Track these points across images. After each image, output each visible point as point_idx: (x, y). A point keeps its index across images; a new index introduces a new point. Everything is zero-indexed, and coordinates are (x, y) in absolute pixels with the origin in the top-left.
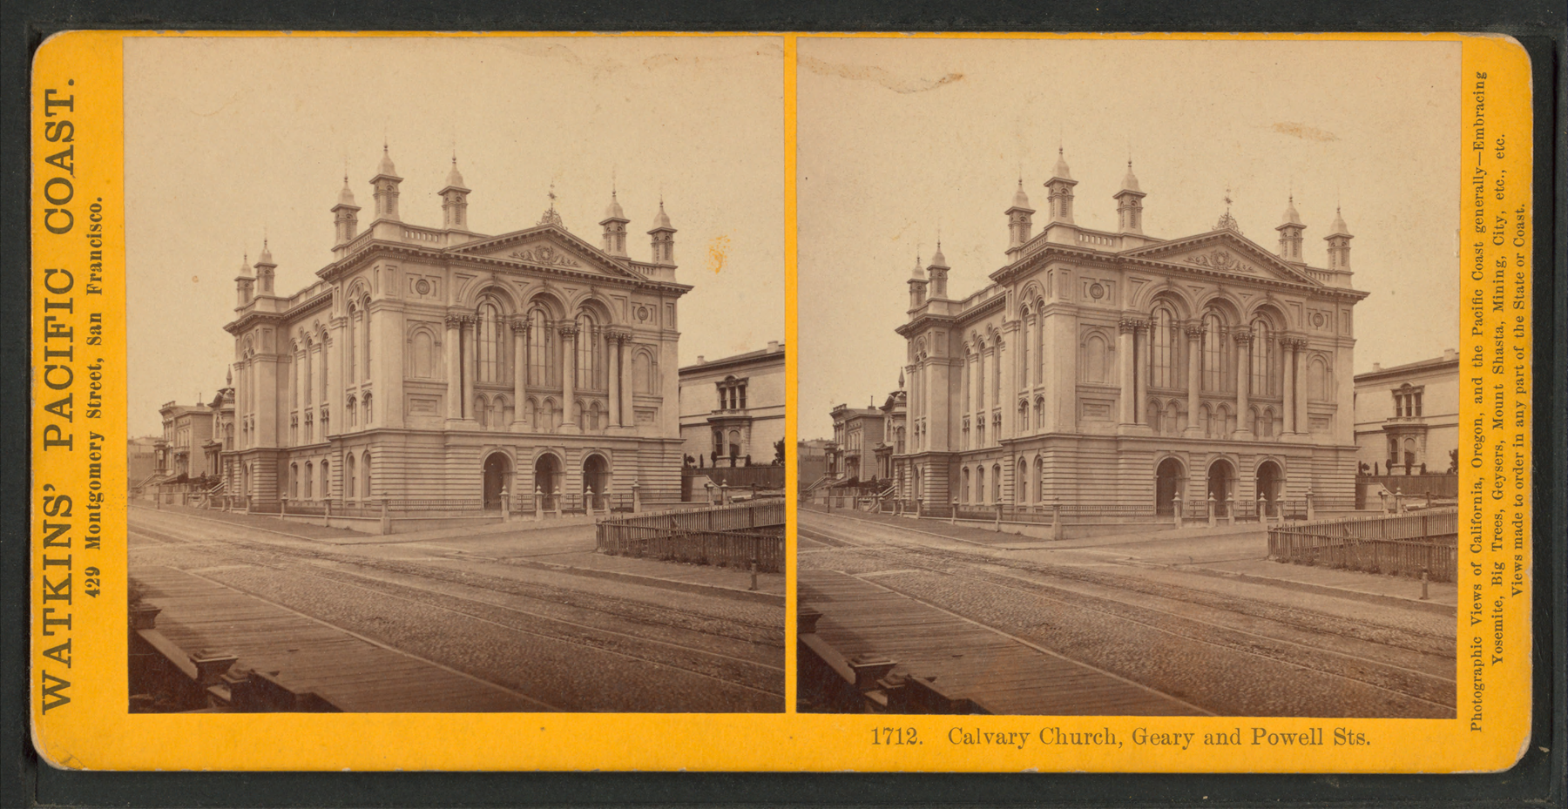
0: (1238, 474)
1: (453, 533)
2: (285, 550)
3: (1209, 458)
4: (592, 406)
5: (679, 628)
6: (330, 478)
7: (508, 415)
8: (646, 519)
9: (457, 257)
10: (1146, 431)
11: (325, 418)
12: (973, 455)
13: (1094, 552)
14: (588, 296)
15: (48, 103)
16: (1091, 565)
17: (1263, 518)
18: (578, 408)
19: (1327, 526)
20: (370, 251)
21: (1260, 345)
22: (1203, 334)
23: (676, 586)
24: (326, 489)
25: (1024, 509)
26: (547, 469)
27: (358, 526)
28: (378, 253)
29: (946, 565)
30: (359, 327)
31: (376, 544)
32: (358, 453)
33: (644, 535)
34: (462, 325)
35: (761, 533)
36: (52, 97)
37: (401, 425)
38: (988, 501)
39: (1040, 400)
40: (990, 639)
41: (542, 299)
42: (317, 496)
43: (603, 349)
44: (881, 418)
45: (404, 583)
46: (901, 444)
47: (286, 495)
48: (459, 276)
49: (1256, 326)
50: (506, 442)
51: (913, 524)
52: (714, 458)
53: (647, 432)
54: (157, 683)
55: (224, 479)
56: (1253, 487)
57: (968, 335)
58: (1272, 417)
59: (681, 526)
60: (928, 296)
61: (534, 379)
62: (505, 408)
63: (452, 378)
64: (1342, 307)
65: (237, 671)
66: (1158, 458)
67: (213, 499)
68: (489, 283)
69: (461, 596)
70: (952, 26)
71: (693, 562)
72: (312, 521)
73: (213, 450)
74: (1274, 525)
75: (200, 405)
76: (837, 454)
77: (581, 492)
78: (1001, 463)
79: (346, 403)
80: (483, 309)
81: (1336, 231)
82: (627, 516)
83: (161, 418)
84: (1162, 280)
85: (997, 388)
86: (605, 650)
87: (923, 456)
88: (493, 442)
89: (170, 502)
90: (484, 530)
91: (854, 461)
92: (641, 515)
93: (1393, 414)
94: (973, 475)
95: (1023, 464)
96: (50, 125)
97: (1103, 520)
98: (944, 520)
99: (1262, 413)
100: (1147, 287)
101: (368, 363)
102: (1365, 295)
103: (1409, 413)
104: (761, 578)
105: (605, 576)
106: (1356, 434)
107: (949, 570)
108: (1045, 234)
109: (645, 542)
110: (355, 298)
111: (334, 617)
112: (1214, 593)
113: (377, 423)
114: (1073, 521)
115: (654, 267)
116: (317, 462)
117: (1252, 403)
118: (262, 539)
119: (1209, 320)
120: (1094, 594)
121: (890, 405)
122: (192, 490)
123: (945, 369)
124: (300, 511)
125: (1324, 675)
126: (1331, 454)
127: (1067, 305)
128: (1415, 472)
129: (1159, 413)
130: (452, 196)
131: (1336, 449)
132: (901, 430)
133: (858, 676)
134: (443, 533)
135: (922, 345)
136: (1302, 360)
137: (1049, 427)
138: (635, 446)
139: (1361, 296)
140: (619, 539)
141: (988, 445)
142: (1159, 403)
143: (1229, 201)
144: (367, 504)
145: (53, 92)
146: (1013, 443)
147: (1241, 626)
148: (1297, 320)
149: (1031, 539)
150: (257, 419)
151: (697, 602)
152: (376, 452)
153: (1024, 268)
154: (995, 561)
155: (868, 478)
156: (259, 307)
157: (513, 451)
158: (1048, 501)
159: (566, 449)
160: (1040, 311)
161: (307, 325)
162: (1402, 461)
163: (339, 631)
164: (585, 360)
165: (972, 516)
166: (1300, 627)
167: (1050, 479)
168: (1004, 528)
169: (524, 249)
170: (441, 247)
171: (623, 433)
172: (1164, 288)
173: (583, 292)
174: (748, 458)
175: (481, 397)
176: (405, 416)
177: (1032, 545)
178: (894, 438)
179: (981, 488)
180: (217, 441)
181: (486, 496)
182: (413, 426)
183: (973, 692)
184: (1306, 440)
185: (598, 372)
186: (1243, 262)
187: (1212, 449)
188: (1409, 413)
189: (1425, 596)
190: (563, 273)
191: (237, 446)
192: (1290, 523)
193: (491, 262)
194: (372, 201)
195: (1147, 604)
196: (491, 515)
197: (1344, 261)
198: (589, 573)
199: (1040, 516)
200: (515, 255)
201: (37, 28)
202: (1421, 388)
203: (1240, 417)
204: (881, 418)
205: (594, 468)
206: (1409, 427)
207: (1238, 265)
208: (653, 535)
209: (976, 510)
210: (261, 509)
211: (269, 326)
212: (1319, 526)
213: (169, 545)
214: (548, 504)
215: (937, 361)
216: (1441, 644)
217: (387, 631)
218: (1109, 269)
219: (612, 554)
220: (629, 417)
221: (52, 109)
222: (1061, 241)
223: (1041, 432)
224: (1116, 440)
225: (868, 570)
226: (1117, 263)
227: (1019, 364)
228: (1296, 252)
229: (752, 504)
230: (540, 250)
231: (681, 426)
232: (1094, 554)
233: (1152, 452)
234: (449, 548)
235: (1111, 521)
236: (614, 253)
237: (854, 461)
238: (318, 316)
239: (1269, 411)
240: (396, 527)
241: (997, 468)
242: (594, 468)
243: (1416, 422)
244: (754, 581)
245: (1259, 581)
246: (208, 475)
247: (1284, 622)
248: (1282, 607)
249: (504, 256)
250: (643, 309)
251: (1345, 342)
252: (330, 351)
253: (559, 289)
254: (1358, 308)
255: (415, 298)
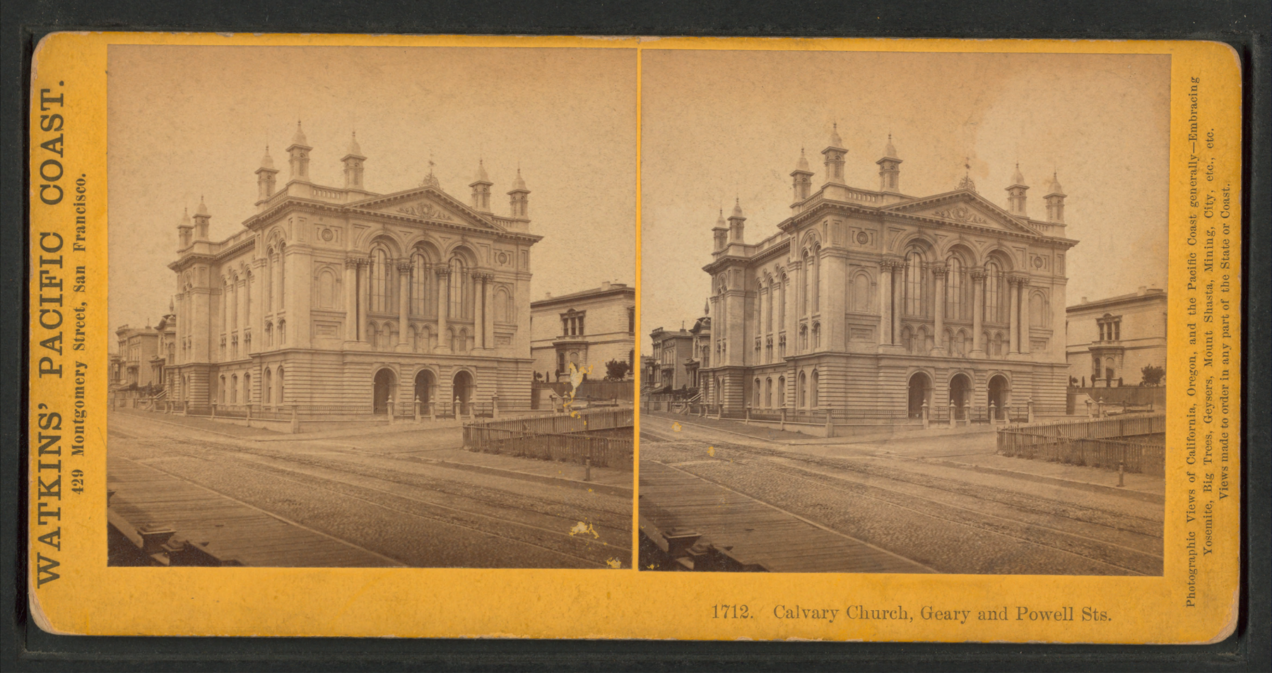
0: (399, 381)
1: (350, 432)
2: (215, 446)
3: (951, 371)
4: (460, 331)
5: (529, 510)
6: (251, 387)
7: (394, 338)
8: (503, 423)
9: (355, 212)
10: (900, 350)
11: (782, 344)
12: (763, 369)
13: (859, 447)
14: (459, 244)
15: (43, 100)
16: (855, 458)
17: (458, 416)
18: (450, 333)
19: (1044, 428)
20: (821, 209)
21: (991, 282)
22: (947, 273)
23: (526, 477)
24: (783, 400)
25: (803, 412)
26: (424, 381)
27: (808, 430)
28: (826, 211)
29: (741, 457)
30: (276, 268)
31: (284, 440)
32: (808, 372)
33: (501, 436)
34: (359, 266)
35: (594, 436)
36: (46, 95)
37: (308, 346)
38: (775, 406)
39: (817, 325)
40: (774, 516)
41: (423, 246)
42: (240, 401)
43: (471, 288)
44: (690, 339)
45: (308, 472)
46: (706, 359)
47: (751, 404)
48: (892, 230)
49: (989, 267)
50: (392, 360)
51: (714, 423)
52: (1093, 379)
53: (505, 353)
54: (125, 551)
55: (167, 388)
56: (412, 390)
57: (760, 273)
58: (1001, 339)
59: (530, 429)
60: (728, 241)
61: (950, 314)
62: (391, 333)
63: (884, 313)
64: (521, 247)
65: (176, 542)
66: (910, 372)
67: (157, 404)
68: (380, 233)
69: (355, 483)
70: (399, 29)
71: (539, 458)
72: (236, 422)
73: (158, 364)
74: (1002, 427)
75: (148, 328)
76: (655, 367)
77: (451, 401)
78: (251, 372)
79: (799, 330)
80: (376, 253)
81: (517, 187)
82: (488, 420)
83: (651, 341)
84: (380, 226)
85: (783, 316)
86: (468, 528)
87: (724, 369)
88: (383, 360)
89: (657, 409)
90: (376, 430)
91: (668, 373)
92: (1034, 425)
93: (561, 333)
94: (763, 386)
95: (803, 376)
96: (44, 117)
97: (867, 422)
98: (740, 421)
99: (993, 337)
100: (902, 235)
101: (283, 298)
102: (539, 238)
103: (574, 333)
104: (594, 471)
105: (471, 468)
106: (1068, 354)
107: (744, 461)
108: (821, 192)
109: (501, 441)
110: (273, 243)
111: (784, 503)
112: (954, 481)
113: (290, 344)
114: (307, 418)
115: (511, 221)
116: (775, 378)
117: (450, 325)
118: (196, 436)
119: (951, 262)
120: (326, 477)
121: (697, 328)
122: (675, 399)
123: (742, 300)
124: (229, 414)
125: (1041, 547)
126: (512, 366)
127: (303, 246)
128: (1114, 384)
129: (911, 336)
130: (887, 165)
131: (517, 361)
132: (706, 348)
133: (145, 542)
134: (341, 433)
135: (723, 280)
136: (489, 288)
137: (824, 347)
138: (495, 365)
139: (1072, 244)
140: (481, 439)
141: (775, 361)
142: (909, 329)
143: (968, 166)
144: (815, 413)
145: (48, 91)
146: (260, 356)
147: (975, 507)
148: (1021, 262)
149: (811, 437)
150: (193, 341)
151: (538, 490)
152: (823, 371)
153: (270, 217)
154: (780, 454)
155: (680, 388)
156: (198, 250)
157: (397, 367)
158: (823, 406)
159: (975, 371)
160: (817, 254)
161: (235, 264)
162: (1104, 376)
163: (788, 514)
164: (456, 295)
165: (229, 414)
166: (1022, 509)
167: (824, 389)
168: (788, 428)
169: (408, 205)
170: (877, 206)
171: (485, 354)
172: (916, 236)
173: (456, 240)
174: (1121, 380)
175: (908, 328)
176: (312, 339)
177: (275, 437)
178: (701, 355)
179: (769, 396)
180: (161, 357)
181: (375, 403)
182: (317, 347)
183: (758, 559)
184: (1028, 359)
185: (466, 305)
186: (979, 216)
187: (418, 361)
188: (574, 333)
189: (1121, 484)
190: (440, 225)
191: (712, 364)
192: (1015, 425)
193: (382, 216)
194: (288, 165)
195: (899, 489)
196: (914, 422)
197: (1059, 215)
198: (457, 466)
199: (816, 418)
200: (401, 210)
201: (29, 29)
202: (584, 312)
203: (976, 340)
204: (690, 339)
205: (462, 382)
206: (1110, 349)
207: (439, 214)
208: (508, 436)
209: (230, 409)
210: (196, 412)
211: (203, 265)
212: (1037, 428)
213: (655, 444)
214: (424, 410)
215: (735, 293)
216: (1134, 523)
217: (825, 515)
218: (337, 217)
219: (1009, 455)
220: (490, 343)
221: (46, 105)
222: (835, 198)
223: (817, 350)
224: (877, 358)
225: (679, 460)
226: (878, 216)
227: (800, 294)
228: (1021, 208)
229: (1122, 417)
230: (422, 206)
231: (532, 349)
232: (851, 449)
233: (450, 367)
234: (347, 445)
235: (873, 422)
236: (480, 209)
237: (668, 373)
238: (776, 261)
239: (464, 330)
240: (304, 427)
241: (782, 380)
242: (462, 382)
243: (1115, 344)
244: (588, 474)
245: (989, 471)
246: (154, 384)
247: (1010, 505)
248: (476, 487)
249: (393, 211)
250: (1038, 258)
251: (524, 275)
252: (253, 285)
253: (436, 238)
254: (1070, 252)
255: (321, 244)
